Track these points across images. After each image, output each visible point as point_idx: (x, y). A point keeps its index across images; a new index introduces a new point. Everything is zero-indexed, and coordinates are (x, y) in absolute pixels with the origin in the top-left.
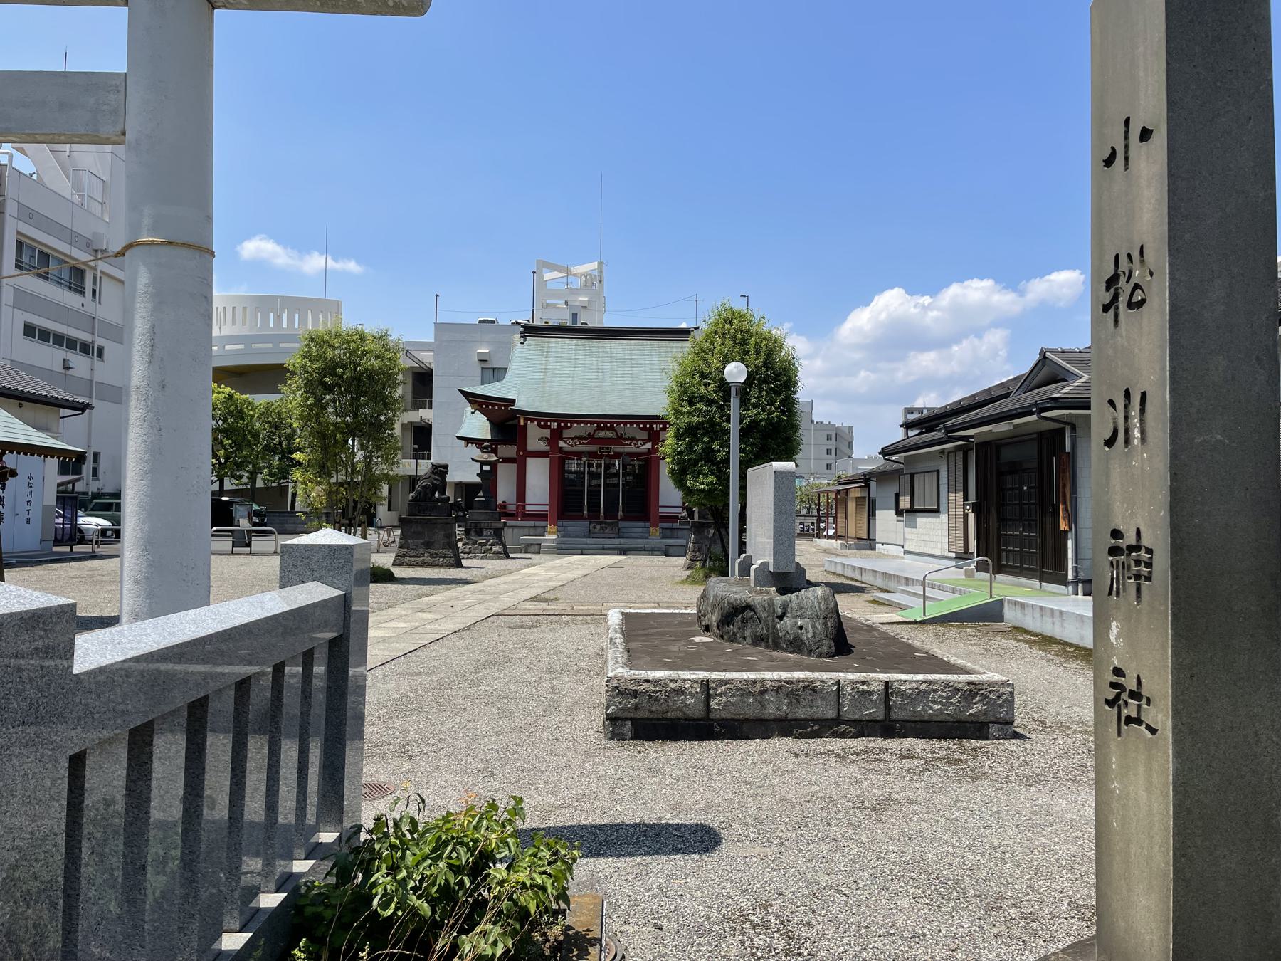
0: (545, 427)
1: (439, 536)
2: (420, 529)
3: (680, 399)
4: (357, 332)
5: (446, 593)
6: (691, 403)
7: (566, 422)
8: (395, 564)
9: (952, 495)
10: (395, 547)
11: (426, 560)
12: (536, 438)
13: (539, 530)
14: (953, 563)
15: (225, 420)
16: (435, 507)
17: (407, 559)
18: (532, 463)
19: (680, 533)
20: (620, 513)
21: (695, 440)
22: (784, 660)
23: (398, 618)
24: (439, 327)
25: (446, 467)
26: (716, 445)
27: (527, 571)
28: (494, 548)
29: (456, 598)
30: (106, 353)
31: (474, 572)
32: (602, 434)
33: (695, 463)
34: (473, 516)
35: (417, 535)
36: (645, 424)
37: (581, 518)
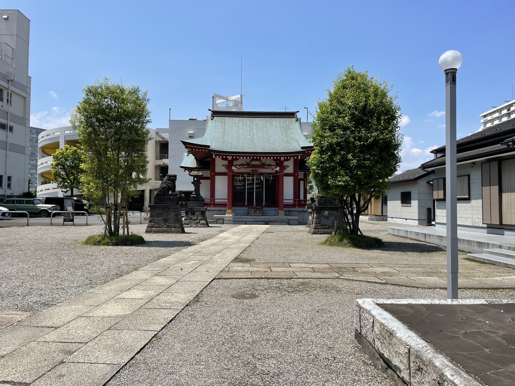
0: (226, 159)
1: (172, 215)
2: (161, 212)
3: (323, 129)
4: (119, 87)
5: (177, 254)
6: (332, 129)
7: (236, 156)
8: (147, 232)
9: (486, 189)
10: (148, 221)
11: (165, 229)
12: (220, 165)
13: (222, 212)
14: (486, 230)
15: (73, 162)
16: (169, 199)
17: (154, 229)
18: (218, 179)
19: (293, 213)
20: (264, 203)
21: (334, 154)
22: (118, 196)
23: (137, 285)
24: (172, 122)
25: (175, 176)
26: (350, 156)
27: (222, 235)
28: (202, 222)
29: (184, 260)
30: (14, 129)
31: (193, 236)
32: (254, 163)
33: (334, 168)
34: (191, 204)
35: (159, 215)
36: (277, 157)
37: (244, 206)
